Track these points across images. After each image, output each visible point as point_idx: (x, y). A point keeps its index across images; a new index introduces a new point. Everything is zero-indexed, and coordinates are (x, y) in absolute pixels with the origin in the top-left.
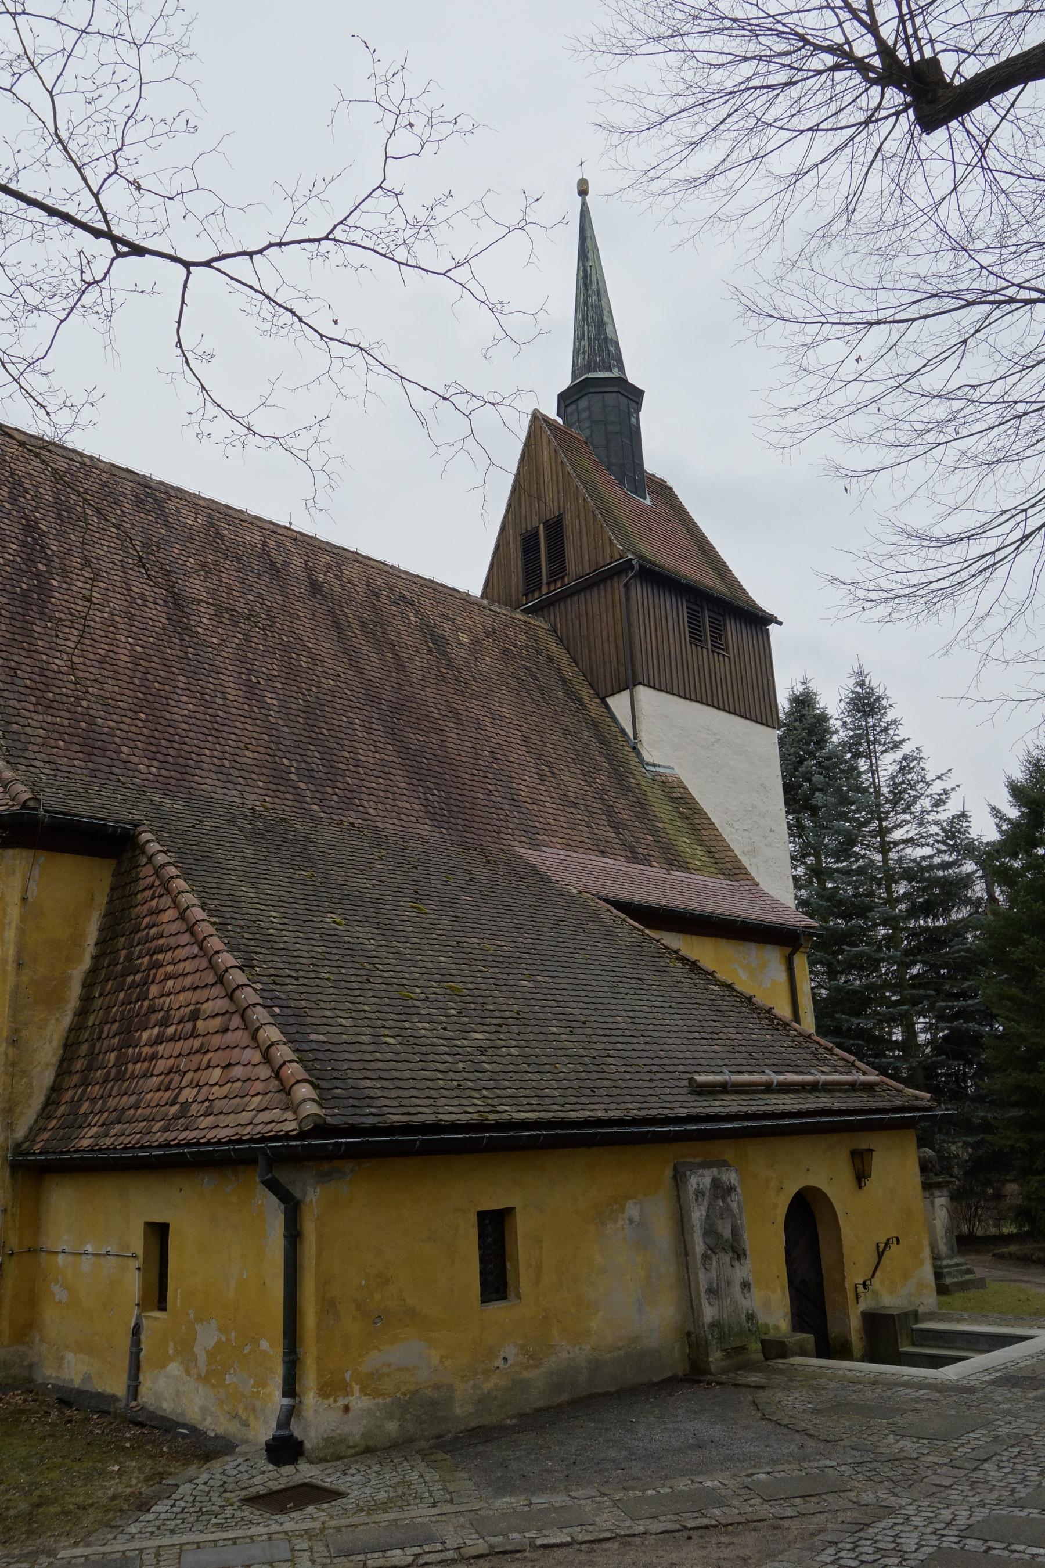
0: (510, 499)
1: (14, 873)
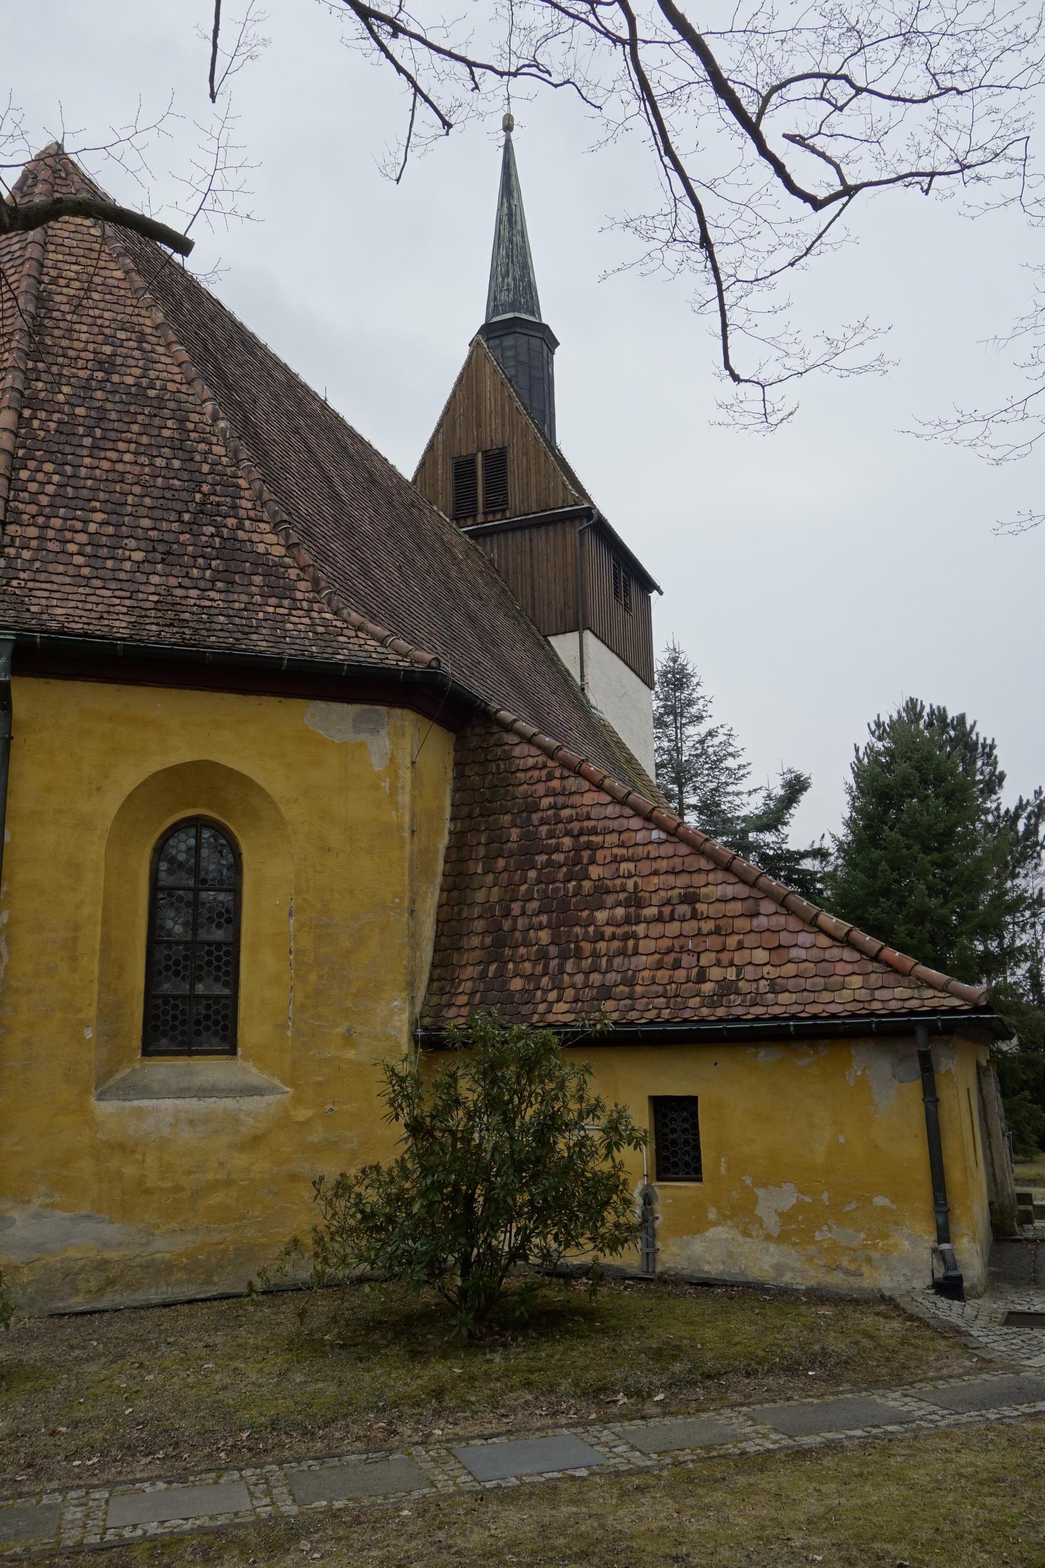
0: (442, 419)
1: (403, 735)
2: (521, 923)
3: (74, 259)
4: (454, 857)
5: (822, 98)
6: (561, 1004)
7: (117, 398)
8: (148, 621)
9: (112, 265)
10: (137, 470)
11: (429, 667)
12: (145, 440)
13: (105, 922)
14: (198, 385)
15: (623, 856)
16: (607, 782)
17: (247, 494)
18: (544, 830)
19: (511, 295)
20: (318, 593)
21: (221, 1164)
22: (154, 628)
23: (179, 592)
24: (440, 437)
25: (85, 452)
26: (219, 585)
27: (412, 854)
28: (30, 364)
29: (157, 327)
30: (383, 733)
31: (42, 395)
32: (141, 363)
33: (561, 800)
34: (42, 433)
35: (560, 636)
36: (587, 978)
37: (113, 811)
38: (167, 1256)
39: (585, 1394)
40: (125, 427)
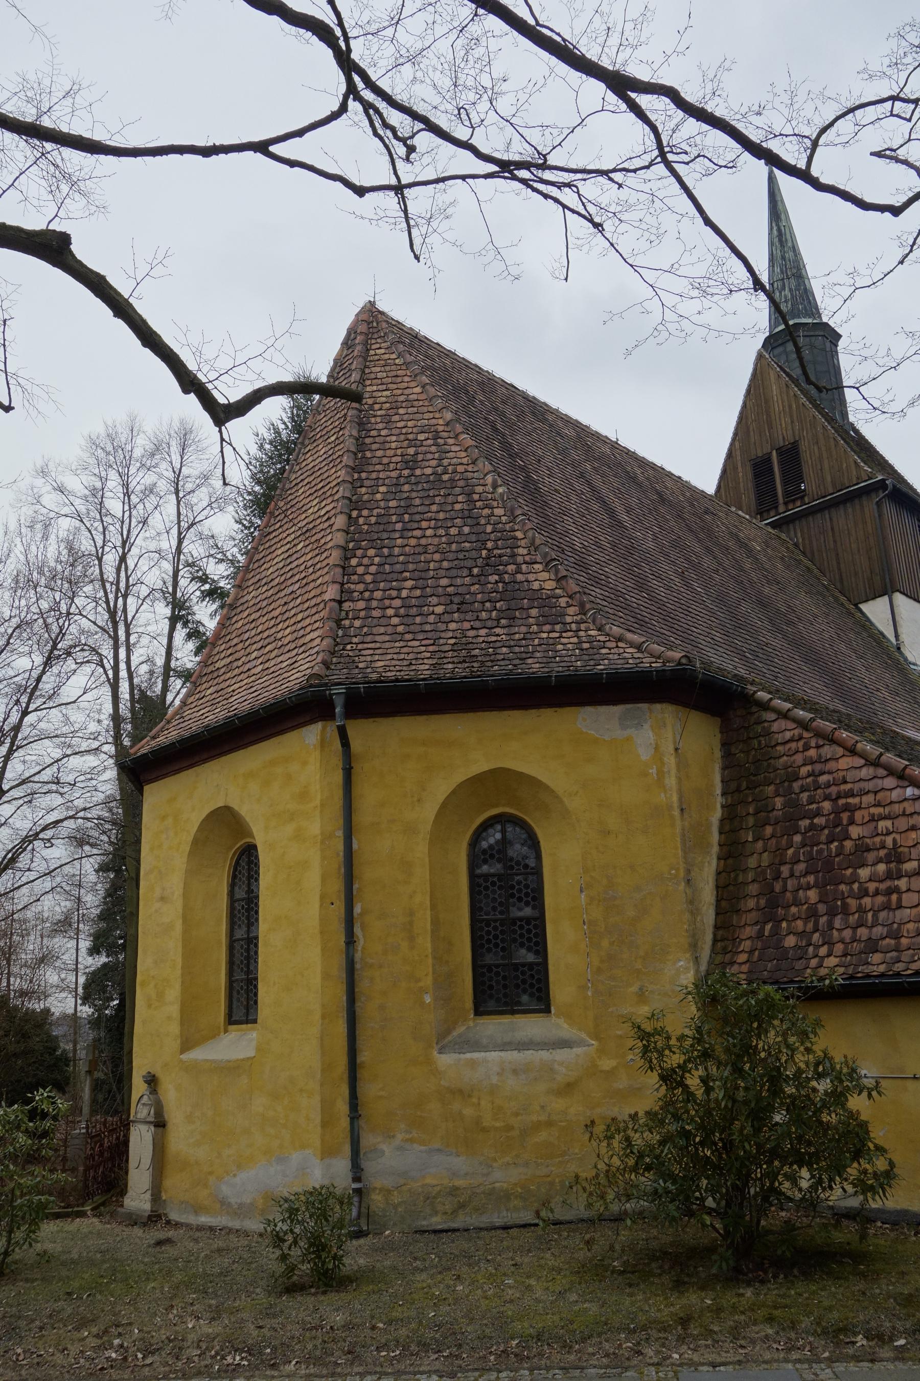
1: (665, 725)
2: (791, 884)
3: (384, 387)
4: (727, 828)
5: (892, 115)
6: (832, 958)
7: (420, 487)
8: (445, 661)
9: (413, 384)
10: (436, 541)
11: (679, 664)
12: (441, 516)
13: (433, 907)
14: (480, 464)
15: (880, 814)
16: (859, 745)
17: (523, 543)
18: (805, 796)
19: (789, 305)
20: (585, 614)
21: (542, 1107)
22: (450, 666)
23: (472, 633)
24: (737, 444)
25: (397, 535)
26: (503, 622)
27: (683, 829)
28: (356, 476)
29: (447, 424)
30: (646, 726)
31: (366, 497)
32: (437, 456)
33: (818, 767)
34: (366, 527)
35: (870, 602)
36: (854, 933)
37: (432, 817)
38: (505, 1185)
39: (825, 1332)
40: (426, 509)
